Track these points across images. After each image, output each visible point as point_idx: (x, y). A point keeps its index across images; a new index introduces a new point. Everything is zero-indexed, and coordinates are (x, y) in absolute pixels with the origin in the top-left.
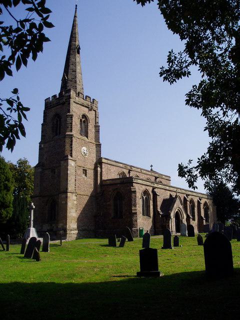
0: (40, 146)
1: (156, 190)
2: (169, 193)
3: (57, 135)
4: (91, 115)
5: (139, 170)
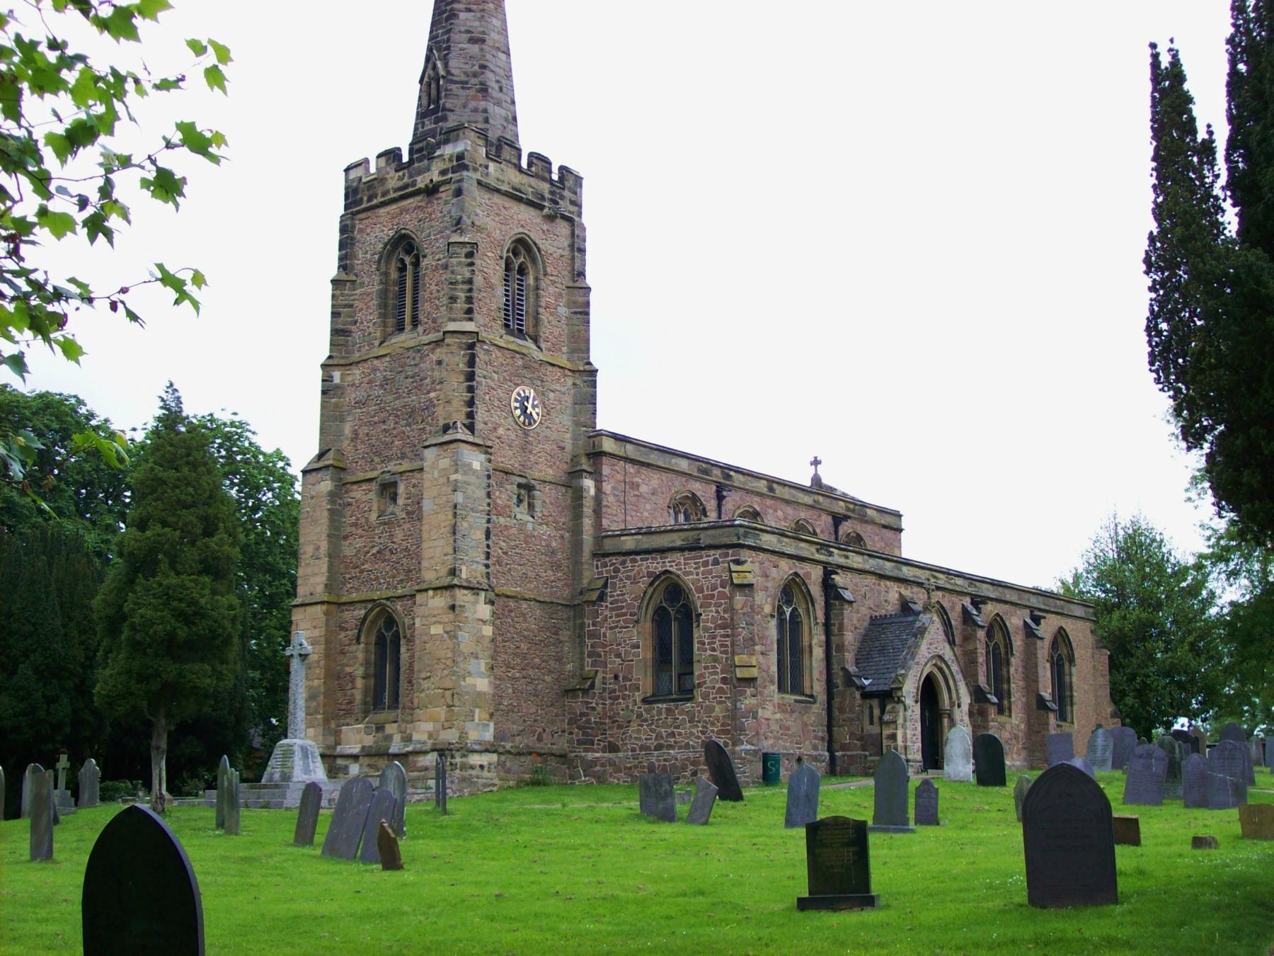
0: (326, 380)
1: (838, 579)
2: (893, 593)
3: (400, 328)
4: (551, 242)
5: (762, 486)
